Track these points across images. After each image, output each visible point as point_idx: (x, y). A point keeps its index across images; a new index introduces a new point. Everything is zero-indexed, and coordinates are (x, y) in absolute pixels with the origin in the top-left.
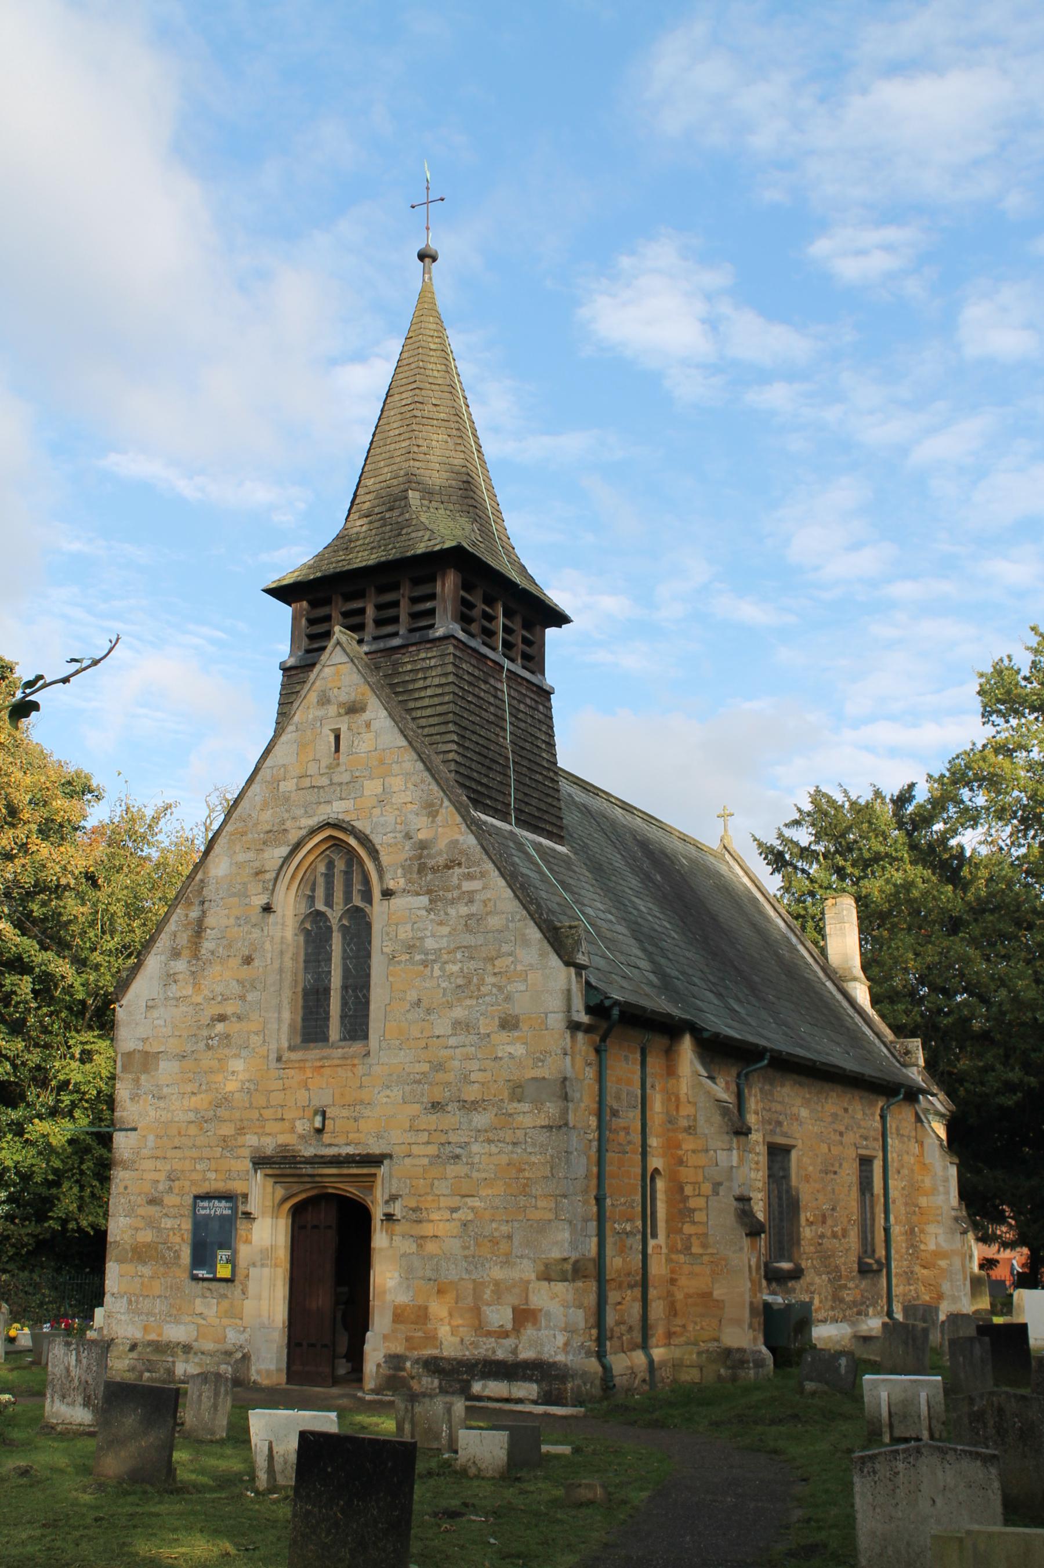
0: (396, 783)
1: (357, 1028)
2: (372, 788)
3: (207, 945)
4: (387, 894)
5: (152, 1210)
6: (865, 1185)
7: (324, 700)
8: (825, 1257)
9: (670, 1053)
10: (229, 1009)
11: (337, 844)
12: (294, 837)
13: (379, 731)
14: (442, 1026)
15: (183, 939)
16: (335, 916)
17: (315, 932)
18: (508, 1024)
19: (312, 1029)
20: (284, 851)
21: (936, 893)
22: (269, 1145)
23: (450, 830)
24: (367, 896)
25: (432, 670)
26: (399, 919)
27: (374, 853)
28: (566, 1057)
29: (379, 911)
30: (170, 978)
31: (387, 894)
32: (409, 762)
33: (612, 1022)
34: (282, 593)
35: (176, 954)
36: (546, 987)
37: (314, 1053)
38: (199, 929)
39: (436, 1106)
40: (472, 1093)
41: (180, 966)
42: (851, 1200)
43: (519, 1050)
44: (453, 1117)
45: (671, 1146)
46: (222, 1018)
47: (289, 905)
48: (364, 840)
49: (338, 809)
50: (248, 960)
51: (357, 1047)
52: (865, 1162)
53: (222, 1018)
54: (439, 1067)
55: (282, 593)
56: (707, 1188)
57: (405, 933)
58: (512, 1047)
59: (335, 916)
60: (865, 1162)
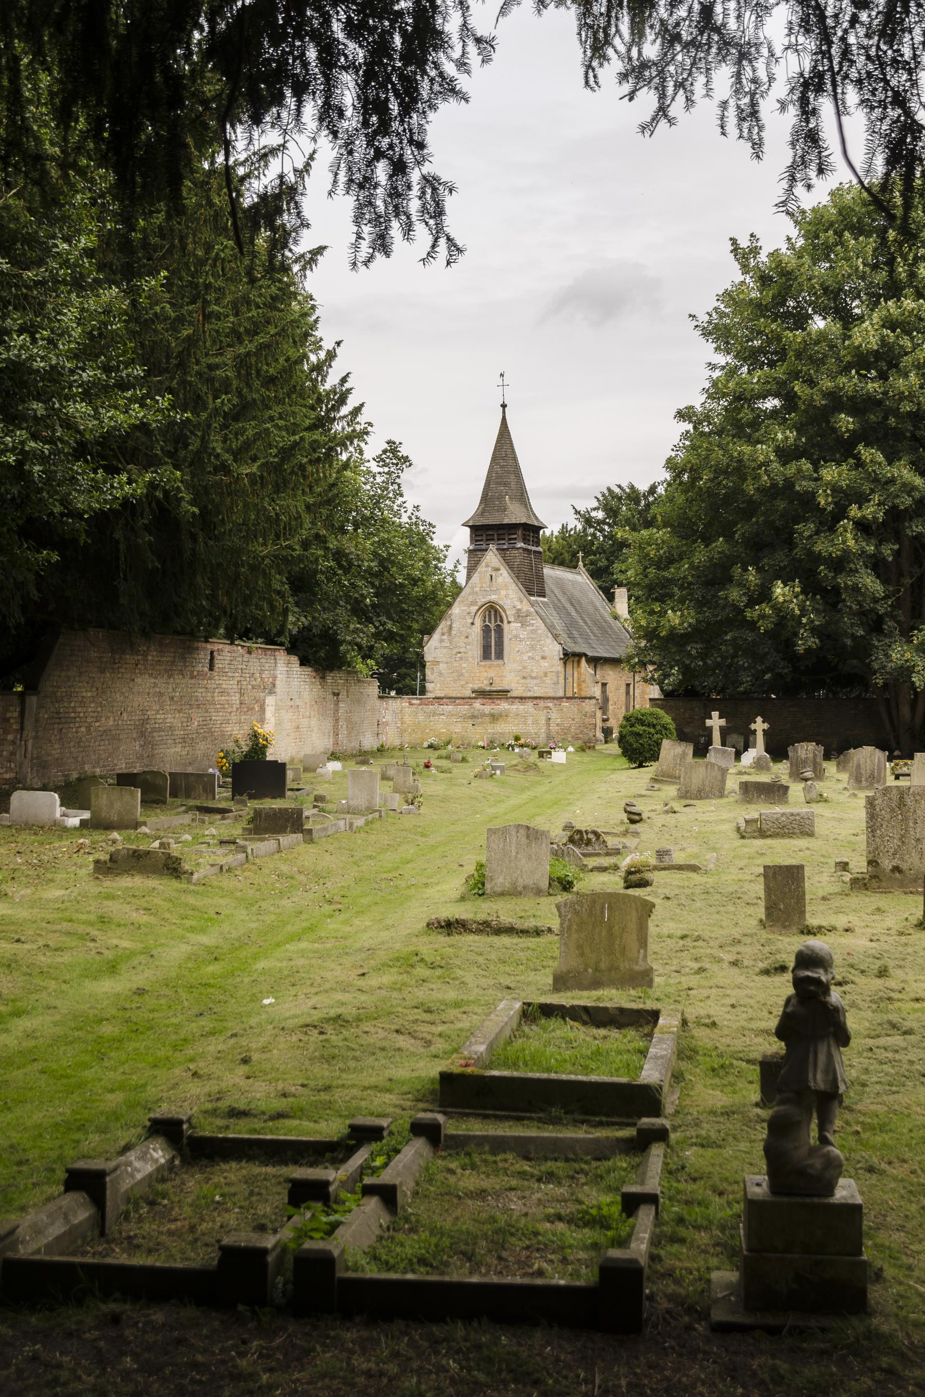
0: (510, 592)
1: (500, 655)
2: (503, 592)
3: (454, 632)
4: (509, 622)
6: (628, 693)
7: (487, 566)
8: (615, 715)
9: (579, 662)
11: (492, 607)
12: (480, 604)
13: (505, 576)
14: (525, 658)
15: (445, 630)
16: (492, 626)
17: (486, 630)
18: (543, 658)
19: (486, 655)
21: (590, 970)
22: (476, 687)
23: (525, 607)
24: (502, 621)
25: (517, 557)
26: (511, 629)
27: (505, 611)
28: (559, 667)
29: (505, 626)
30: (442, 641)
31: (509, 622)
32: (514, 586)
33: (570, 657)
35: (443, 634)
36: (555, 650)
37: (488, 663)
38: (450, 628)
40: (534, 675)
42: (623, 697)
44: (529, 681)
45: (579, 685)
47: (478, 622)
48: (501, 607)
49: (493, 597)
51: (500, 662)
52: (628, 685)
54: (525, 668)
57: (514, 633)
58: (545, 664)
59: (492, 626)
60: (628, 685)
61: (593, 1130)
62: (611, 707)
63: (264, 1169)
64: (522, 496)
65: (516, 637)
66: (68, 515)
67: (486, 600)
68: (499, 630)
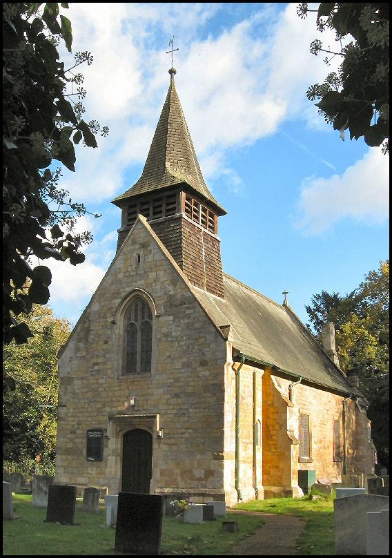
0: (161, 273)
3: (91, 337)
5: (72, 436)
7: (134, 243)
10: (100, 360)
12: (123, 295)
16: (138, 325)
17: (130, 330)
19: (129, 367)
20: (119, 301)
24: (150, 316)
34: (118, 203)
37: (131, 376)
39: (177, 396)
41: (81, 345)
43: (207, 373)
46: (97, 364)
49: (138, 285)
50: (106, 342)
53: (97, 364)
55: (118, 203)
56: (277, 427)
57: (164, 330)
59: (138, 325)
61: (268, 355)
62: (314, 447)
63: (318, 372)
64: (188, 160)
65: (167, 335)
66: (208, 419)
67: (128, 289)
68: (147, 328)
